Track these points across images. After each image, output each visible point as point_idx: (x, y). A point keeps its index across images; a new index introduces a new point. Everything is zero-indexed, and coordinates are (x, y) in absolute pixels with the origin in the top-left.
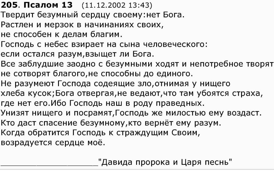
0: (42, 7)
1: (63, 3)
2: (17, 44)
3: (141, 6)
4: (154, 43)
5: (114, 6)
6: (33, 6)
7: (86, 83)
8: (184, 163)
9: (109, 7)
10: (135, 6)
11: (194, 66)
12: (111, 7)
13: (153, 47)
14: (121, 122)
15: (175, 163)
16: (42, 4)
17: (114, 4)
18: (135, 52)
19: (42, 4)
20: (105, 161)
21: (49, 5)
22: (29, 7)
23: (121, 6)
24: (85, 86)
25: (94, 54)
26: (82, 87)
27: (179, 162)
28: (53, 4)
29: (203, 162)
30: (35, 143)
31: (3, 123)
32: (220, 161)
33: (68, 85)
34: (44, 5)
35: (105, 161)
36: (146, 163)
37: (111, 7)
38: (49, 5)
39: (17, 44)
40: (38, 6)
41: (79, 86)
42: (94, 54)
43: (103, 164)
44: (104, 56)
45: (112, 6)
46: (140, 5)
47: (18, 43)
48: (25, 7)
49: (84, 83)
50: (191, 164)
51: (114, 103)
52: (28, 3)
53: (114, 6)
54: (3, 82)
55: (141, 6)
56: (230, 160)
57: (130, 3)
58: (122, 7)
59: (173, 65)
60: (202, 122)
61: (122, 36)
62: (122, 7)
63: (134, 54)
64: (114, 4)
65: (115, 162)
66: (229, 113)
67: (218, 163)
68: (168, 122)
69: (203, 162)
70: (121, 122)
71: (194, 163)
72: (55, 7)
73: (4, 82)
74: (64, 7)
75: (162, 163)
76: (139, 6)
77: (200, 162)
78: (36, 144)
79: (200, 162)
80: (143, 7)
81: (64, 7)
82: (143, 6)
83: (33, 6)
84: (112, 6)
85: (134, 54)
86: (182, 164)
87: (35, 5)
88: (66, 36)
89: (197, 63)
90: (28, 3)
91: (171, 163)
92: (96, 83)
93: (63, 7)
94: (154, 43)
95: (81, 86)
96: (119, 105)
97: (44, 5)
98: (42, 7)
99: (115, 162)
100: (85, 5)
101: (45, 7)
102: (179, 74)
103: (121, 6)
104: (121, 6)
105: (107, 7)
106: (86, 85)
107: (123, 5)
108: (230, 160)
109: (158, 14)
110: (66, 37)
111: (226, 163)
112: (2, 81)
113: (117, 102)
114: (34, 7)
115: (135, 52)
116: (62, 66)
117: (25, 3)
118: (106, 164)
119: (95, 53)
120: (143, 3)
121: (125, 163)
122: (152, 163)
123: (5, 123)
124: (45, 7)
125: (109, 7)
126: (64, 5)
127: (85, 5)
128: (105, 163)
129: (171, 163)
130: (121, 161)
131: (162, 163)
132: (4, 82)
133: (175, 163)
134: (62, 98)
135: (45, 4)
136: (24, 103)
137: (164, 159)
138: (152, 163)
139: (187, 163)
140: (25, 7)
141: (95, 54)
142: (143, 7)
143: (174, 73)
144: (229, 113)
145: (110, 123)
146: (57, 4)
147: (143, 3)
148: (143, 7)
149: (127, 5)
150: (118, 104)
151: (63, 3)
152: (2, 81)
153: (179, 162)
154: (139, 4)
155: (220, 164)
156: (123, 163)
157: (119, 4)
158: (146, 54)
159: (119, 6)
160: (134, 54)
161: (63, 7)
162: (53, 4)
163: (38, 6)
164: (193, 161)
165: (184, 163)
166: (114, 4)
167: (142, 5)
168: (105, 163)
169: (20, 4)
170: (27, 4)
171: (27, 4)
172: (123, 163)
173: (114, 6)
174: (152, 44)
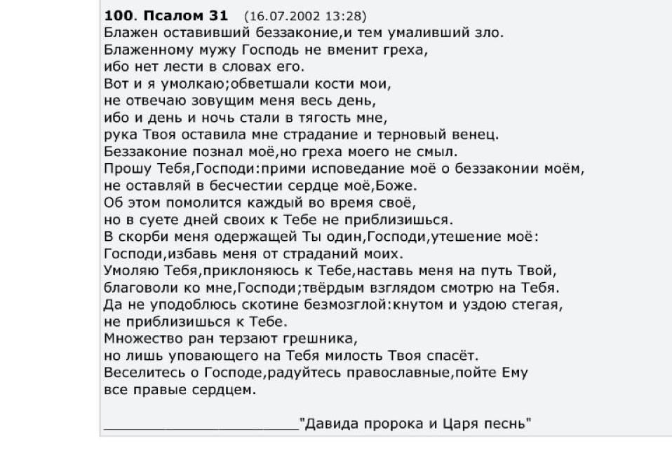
0: (175, 19)
6: (160, 17)
8: (448, 424)
10: (336, 18)
15: (433, 424)
16: (176, 14)
17: (301, 14)
19: (176, 14)
20: (311, 421)
21: (187, 17)
22: (152, 19)
27: (440, 424)
28: (195, 14)
29: (481, 424)
32: (511, 422)
34: (178, 16)
35: (311, 421)
36: (381, 424)
38: (187, 17)
43: (307, 427)
45: (296, 17)
48: (146, 19)
50: (460, 427)
52: (152, 12)
56: (529, 419)
57: (329, 13)
62: (315, 20)
64: (301, 14)
65: (328, 424)
67: (506, 424)
69: (481, 424)
71: (466, 424)
72: (198, 20)
74: (109, 19)
75: (410, 424)
77: (475, 424)
79: (475, 424)
81: (109, 19)
83: (160, 17)
84: (296, 17)
86: (445, 427)
87: (164, 15)
90: (152, 12)
91: (426, 425)
97: (178, 16)
98: (175, 19)
99: (328, 424)
101: (180, 19)
103: (313, 18)
107: (314, 16)
108: (529, 419)
111: (521, 426)
114: (161, 20)
117: (146, 12)
118: (314, 427)
121: (346, 426)
122: (392, 425)
124: (180, 19)
127: (250, 17)
128: (311, 425)
129: (426, 425)
130: (339, 422)
131: (410, 424)
133: (433, 424)
135: (180, 14)
137: (414, 417)
138: (392, 425)
139: (453, 426)
140: (146, 19)
146: (201, 14)
149: (323, 16)
153: (440, 424)
155: (511, 427)
156: (342, 426)
157: (308, 15)
159: (308, 18)
162: (195, 14)
163: (168, 18)
164: (464, 422)
165: (448, 424)
168: (311, 425)
169: (138, 14)
170: (149, 14)
171: (149, 14)
172: (342, 426)
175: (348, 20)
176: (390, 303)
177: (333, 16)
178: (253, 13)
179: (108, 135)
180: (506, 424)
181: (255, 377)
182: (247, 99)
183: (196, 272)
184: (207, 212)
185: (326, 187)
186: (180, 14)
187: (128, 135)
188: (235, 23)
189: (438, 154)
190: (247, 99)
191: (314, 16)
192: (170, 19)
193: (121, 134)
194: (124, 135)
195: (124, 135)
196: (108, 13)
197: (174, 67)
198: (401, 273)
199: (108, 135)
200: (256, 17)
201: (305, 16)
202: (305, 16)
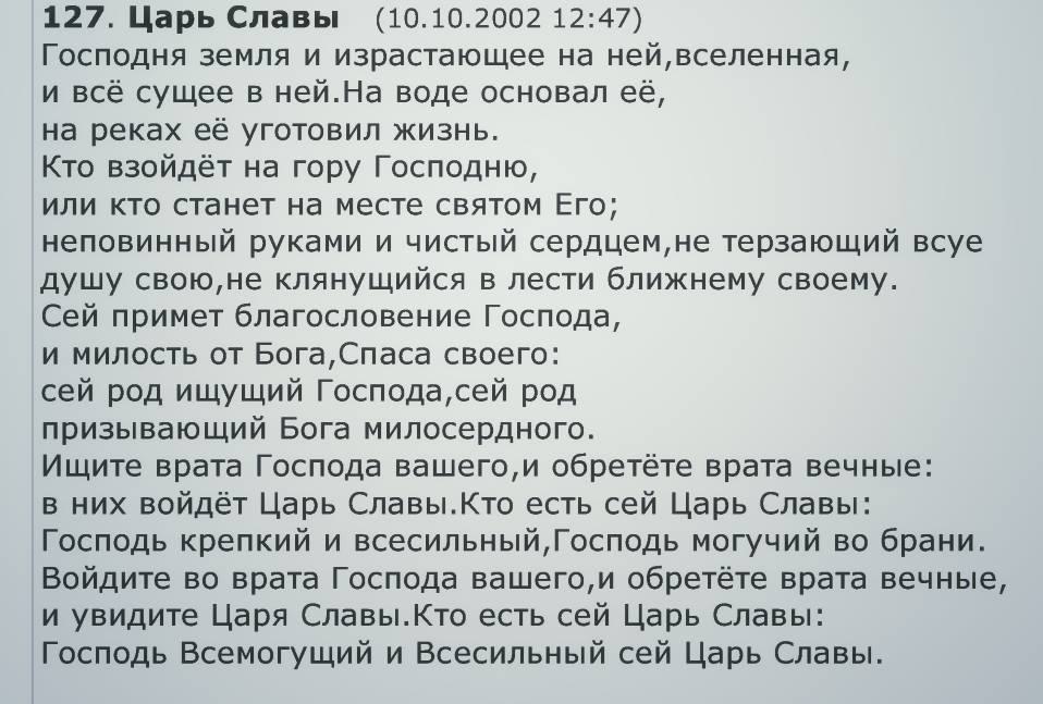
1: (46, 10)
2: (103, 55)
3: (601, 20)
4: (734, 51)
5: (499, 21)
7: (425, 390)
9: (478, 26)
11: (688, 250)
12: (487, 26)
13: (730, 64)
14: (873, 275)
17: (499, 14)
18: (287, 423)
23: (526, 21)
24: (421, 399)
25: (115, 430)
26: (588, 253)
30: (969, 242)
31: (467, 507)
33: (356, 398)
34: (260, 17)
37: (487, 26)
39: (103, 55)
40: (164, 22)
41: (400, 399)
42: (115, 430)
44: (380, 287)
46: (597, 16)
47: (108, 51)
49: (416, 389)
51: (502, 579)
53: (516, 14)
54: (357, 93)
55: (601, 20)
57: (559, 11)
58: (530, 26)
59: (833, 61)
60: (717, 651)
61: (498, 138)
62: (530, 26)
63: (286, 430)
64: (499, 14)
66: (921, 244)
68: (729, 574)
70: (873, 275)
73: (353, 85)
74: (52, 24)
76: (595, 20)
78: (973, 246)
80: (609, 26)
81: (52, 24)
82: (610, 21)
85: (284, 427)
88: (193, 175)
89: (467, 464)
92: (462, 390)
93: (47, 26)
94: (734, 51)
95: (404, 401)
96: (520, 587)
97: (260, 17)
100: (387, 19)
101: (265, 24)
102: (543, 431)
103: (526, 22)
104: (526, 21)
105: (473, 25)
106: (424, 396)
107: (529, 17)
109: (216, 312)
110: (192, 178)
112: (346, 82)
113: (511, 574)
115: (287, 423)
116: (255, 289)
119: (119, 424)
120: (609, 10)
123: (477, 502)
125: (573, 26)
126: (52, 17)
127: (387, 19)
132: (353, 85)
134: (269, 599)
135: (265, 14)
136: (461, 315)
141: (119, 430)
142: (609, 26)
143: (524, 426)
144: (921, 244)
145: (727, 508)
147: (609, 10)
148: (606, 24)
149: (548, 19)
150: (516, 583)
151: (46, 10)
152: (346, 82)
154: (591, 15)
157: (516, 15)
158: (329, 430)
160: (286, 430)
161: (47, 26)
163: (280, 22)
166: (499, 15)
167: (606, 18)
173: (499, 21)
174: (724, 56)
175: (478, 26)
176: (453, 512)
177: (63, 17)
178: (394, 11)
179: (258, 243)
180: (482, 655)
181: (624, 251)
182: (174, 313)
183: (835, 58)
184: (241, 412)
185: (613, 245)
186: (265, 14)
187: (302, 243)
188: (356, 32)
189: (507, 546)
190: (174, 313)
191: (529, 17)
192: (285, 25)
193: (286, 242)
194: (292, 244)
195: (292, 244)
196: (51, 10)
197: (750, 56)
198: (368, 621)
199: (258, 243)
200: (444, 20)
201: (508, 18)
202: (508, 18)
